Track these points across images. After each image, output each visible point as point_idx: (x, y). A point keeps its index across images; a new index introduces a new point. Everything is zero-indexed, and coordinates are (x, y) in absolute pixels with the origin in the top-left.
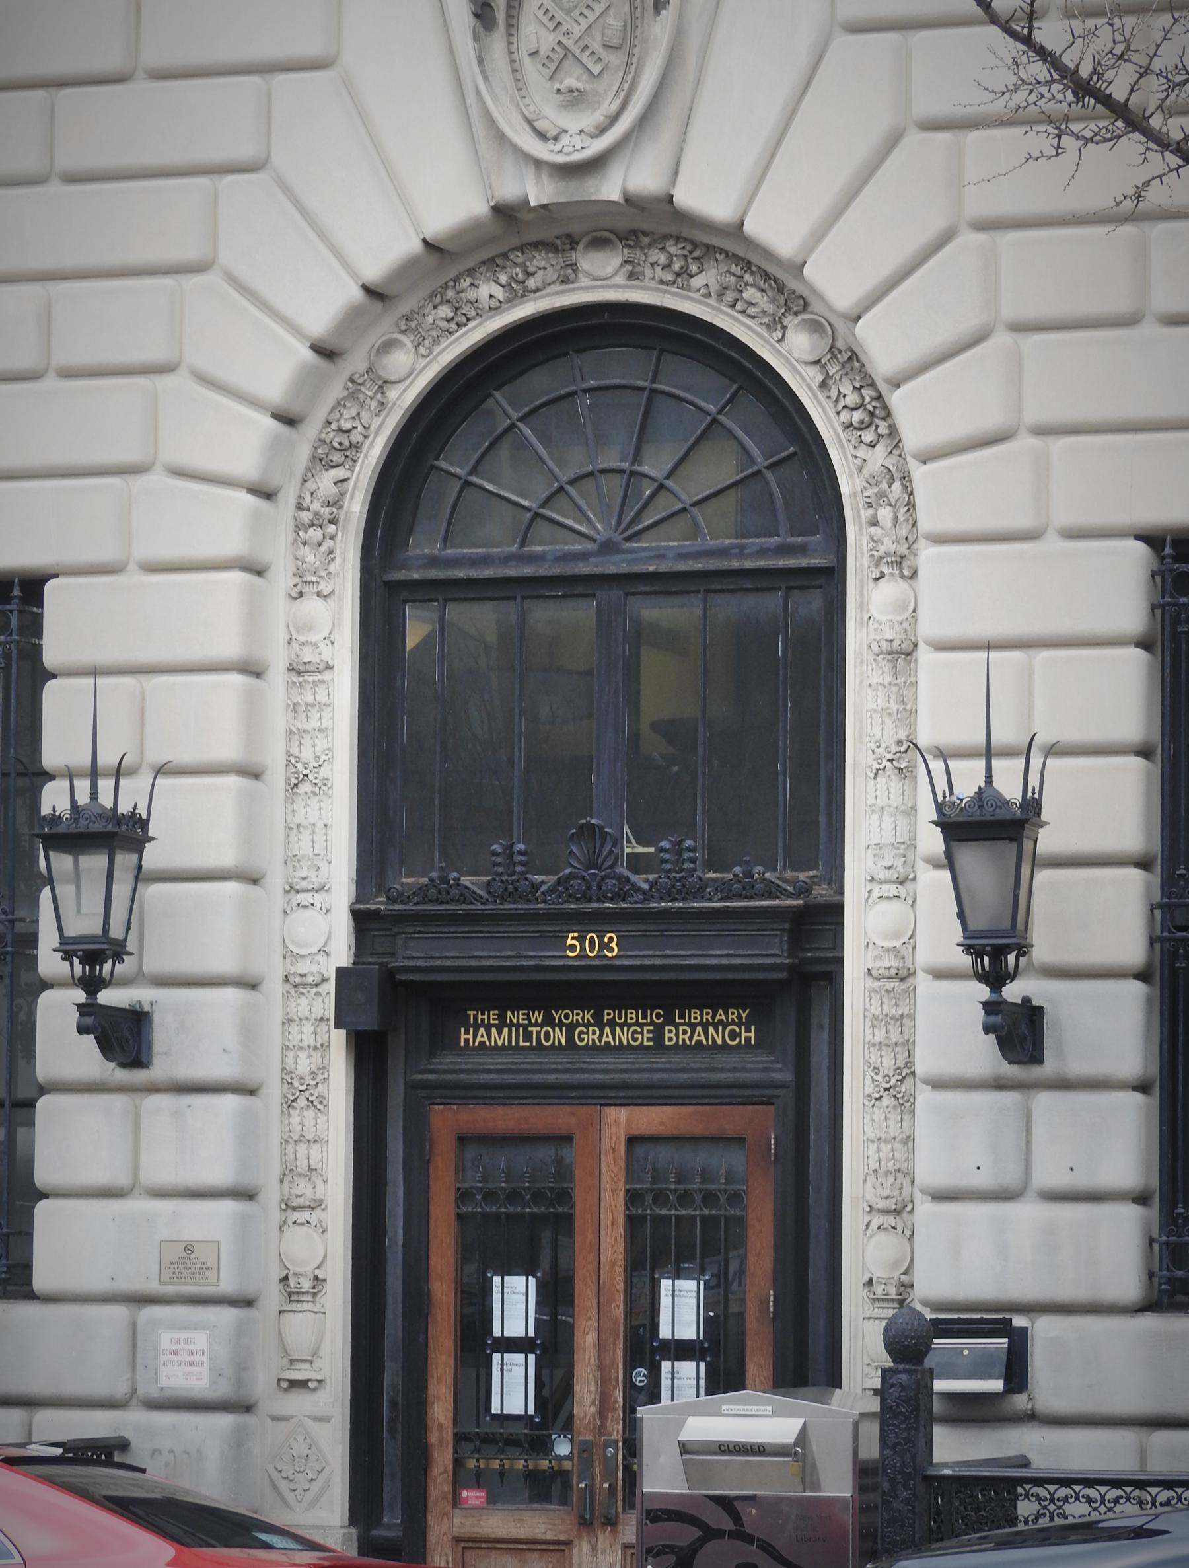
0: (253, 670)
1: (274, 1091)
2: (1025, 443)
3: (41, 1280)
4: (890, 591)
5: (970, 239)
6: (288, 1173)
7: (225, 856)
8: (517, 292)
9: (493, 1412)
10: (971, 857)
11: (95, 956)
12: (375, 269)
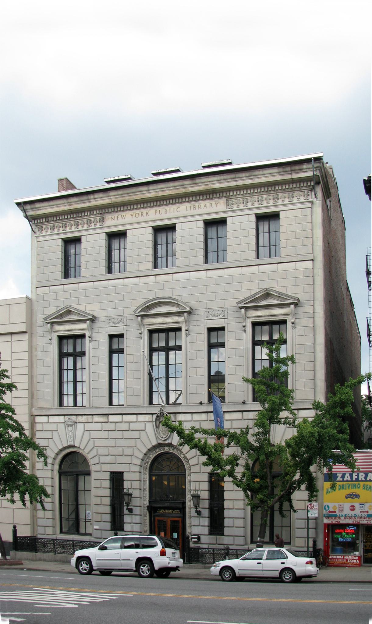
0: (140, 489)
1: (143, 515)
4: (146, 529)
7: (138, 496)
8: (160, 450)
9: (18, 436)
10: (194, 498)
11: (128, 504)
12: (149, 448)
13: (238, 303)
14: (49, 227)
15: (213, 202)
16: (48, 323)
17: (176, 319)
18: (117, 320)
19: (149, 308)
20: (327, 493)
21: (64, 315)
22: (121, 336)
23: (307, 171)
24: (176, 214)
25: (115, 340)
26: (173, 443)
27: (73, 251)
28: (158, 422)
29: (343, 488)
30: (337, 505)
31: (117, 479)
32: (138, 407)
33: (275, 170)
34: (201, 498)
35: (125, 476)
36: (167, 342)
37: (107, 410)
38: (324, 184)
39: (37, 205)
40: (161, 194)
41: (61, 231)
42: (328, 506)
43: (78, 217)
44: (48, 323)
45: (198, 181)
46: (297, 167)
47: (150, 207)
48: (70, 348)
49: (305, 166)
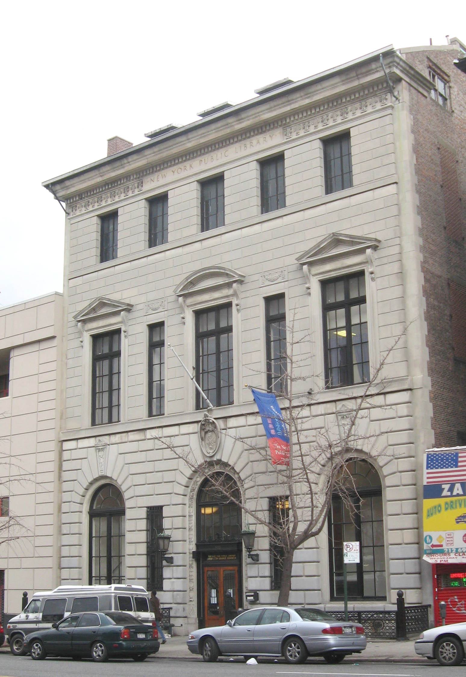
1: (188, 566)
2: (256, 487)
3: (164, 589)
5: (250, 463)
6: (190, 576)
11: (249, 549)
13: (298, 259)
14: (83, 204)
15: (267, 135)
16: (79, 321)
17: (226, 292)
18: (156, 306)
19: (193, 283)
20: (428, 516)
21: (101, 307)
22: (282, 296)
23: (377, 71)
24: (224, 160)
25: (275, 303)
26: (223, 460)
27: (160, 213)
28: (203, 433)
29: (452, 507)
30: (443, 534)
31: (155, 514)
32: (181, 414)
33: (336, 80)
34: (256, 535)
35: (166, 512)
36: (347, 294)
37: (143, 423)
38: (335, 102)
39: (68, 183)
40: (203, 140)
41: (96, 207)
42: (430, 537)
43: (114, 187)
44: (79, 321)
45: (243, 115)
46: (364, 70)
47: (193, 158)
48: (106, 349)
49: (374, 66)
